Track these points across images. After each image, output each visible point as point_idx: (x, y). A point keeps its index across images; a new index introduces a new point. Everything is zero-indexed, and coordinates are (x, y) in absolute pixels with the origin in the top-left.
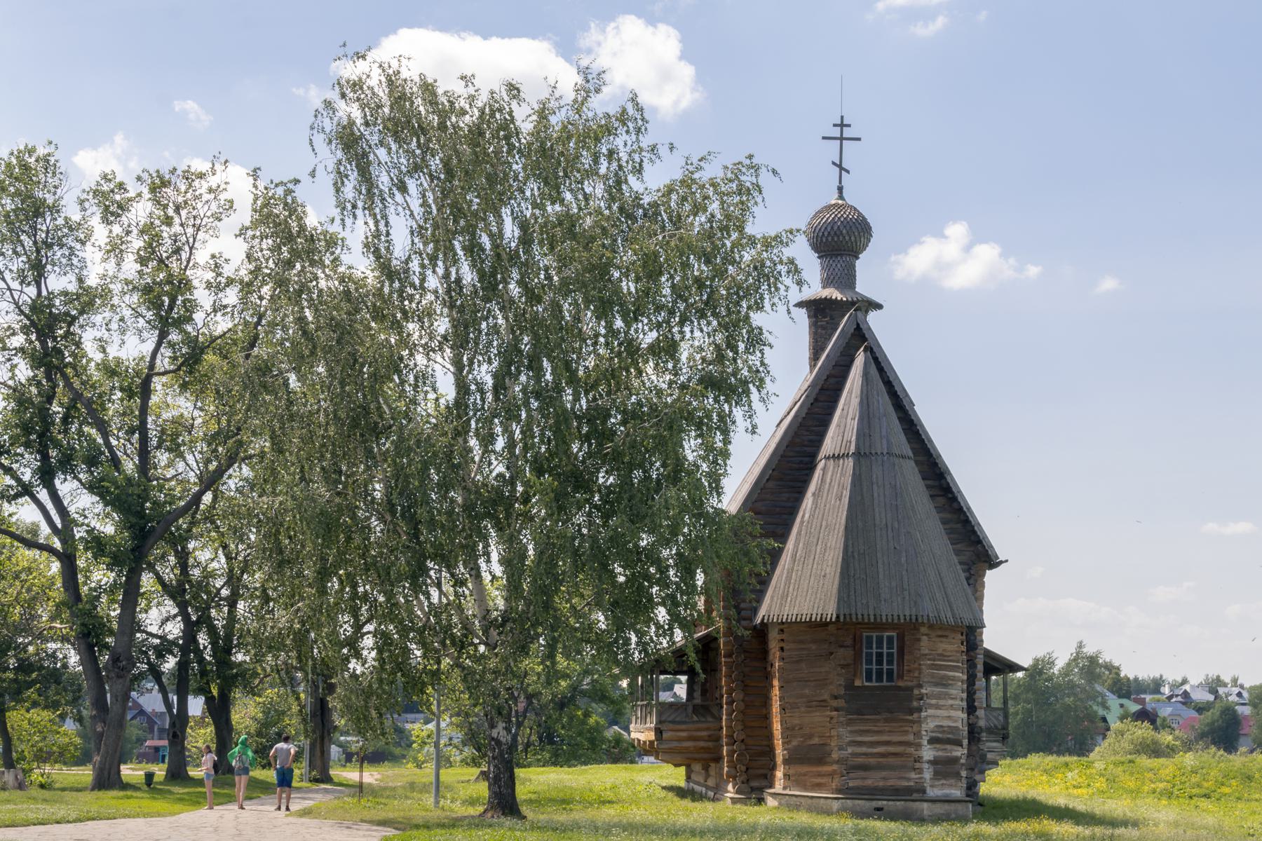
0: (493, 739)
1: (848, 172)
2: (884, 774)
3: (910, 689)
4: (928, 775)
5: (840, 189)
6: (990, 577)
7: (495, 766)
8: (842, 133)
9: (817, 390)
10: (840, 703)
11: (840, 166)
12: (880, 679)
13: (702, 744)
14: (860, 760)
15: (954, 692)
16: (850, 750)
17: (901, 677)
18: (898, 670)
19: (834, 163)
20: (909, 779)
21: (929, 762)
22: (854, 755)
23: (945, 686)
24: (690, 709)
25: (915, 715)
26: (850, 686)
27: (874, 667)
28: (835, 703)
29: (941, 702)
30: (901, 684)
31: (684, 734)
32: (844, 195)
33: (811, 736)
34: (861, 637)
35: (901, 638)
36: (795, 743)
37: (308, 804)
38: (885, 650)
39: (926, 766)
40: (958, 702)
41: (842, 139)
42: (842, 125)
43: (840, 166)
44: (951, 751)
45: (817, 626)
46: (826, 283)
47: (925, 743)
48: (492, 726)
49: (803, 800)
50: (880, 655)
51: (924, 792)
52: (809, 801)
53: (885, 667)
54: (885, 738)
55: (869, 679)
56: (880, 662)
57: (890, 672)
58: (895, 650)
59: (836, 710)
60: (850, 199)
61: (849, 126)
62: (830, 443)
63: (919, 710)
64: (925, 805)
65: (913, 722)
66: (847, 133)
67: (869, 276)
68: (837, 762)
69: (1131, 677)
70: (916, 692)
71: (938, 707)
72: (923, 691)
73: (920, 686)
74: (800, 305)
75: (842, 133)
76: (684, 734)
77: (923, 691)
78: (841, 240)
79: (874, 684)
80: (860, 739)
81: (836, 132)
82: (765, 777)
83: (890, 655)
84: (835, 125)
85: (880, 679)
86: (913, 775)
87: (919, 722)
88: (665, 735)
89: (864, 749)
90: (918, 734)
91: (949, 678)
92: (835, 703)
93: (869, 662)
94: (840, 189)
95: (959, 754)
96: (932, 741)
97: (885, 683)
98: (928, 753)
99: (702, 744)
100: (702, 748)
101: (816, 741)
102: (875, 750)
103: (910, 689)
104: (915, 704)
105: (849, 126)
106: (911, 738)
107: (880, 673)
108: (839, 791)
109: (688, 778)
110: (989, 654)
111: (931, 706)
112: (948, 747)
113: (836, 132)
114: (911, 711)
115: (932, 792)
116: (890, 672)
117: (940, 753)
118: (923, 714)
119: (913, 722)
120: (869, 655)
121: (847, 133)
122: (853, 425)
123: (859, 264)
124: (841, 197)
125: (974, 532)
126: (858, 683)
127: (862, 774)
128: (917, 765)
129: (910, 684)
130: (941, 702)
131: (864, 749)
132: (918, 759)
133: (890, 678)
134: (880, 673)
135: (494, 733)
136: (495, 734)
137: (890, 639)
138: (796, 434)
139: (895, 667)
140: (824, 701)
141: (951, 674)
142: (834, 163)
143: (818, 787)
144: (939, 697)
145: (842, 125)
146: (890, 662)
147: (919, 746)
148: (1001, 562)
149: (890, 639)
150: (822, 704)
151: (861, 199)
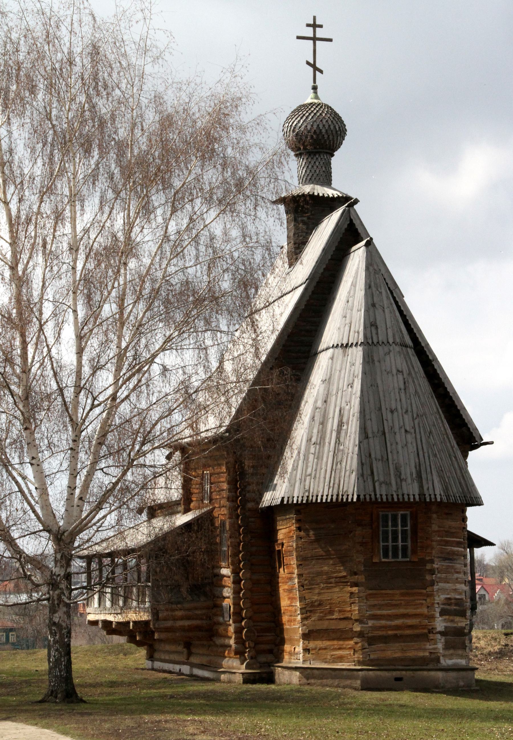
4: (440, 646)
6: (472, 455)
9: (314, 284)
11: (313, 66)
12: (395, 555)
15: (458, 566)
17: (414, 552)
20: (425, 650)
21: (442, 633)
22: (374, 628)
23: (451, 560)
29: (449, 576)
32: (319, 94)
35: (414, 517)
37: (376, 602)
39: (439, 636)
41: (314, 39)
42: (314, 26)
43: (313, 66)
44: (457, 623)
47: (438, 615)
50: (395, 533)
51: (438, 660)
54: (402, 611)
55: (386, 555)
56: (395, 539)
57: (405, 549)
58: (408, 528)
60: (325, 98)
61: (321, 26)
62: (332, 332)
63: (432, 583)
66: (320, 33)
67: (347, 172)
77: (435, 566)
78: (318, 138)
79: (390, 560)
80: (379, 612)
81: (309, 32)
82: (271, 651)
83: (404, 532)
84: (308, 25)
85: (395, 555)
87: (431, 595)
89: (383, 622)
91: (454, 553)
93: (385, 539)
94: (315, 88)
95: (463, 624)
96: (443, 613)
97: (400, 559)
105: (321, 26)
106: (425, 611)
107: (395, 549)
110: (471, 534)
111: (442, 580)
113: (309, 32)
115: (446, 662)
116: (405, 549)
117: (449, 624)
118: (436, 587)
120: (386, 533)
121: (320, 33)
122: (358, 318)
123: (333, 160)
124: (317, 97)
125: (461, 416)
126: (376, 560)
128: (431, 636)
131: (383, 622)
132: (432, 631)
134: (395, 549)
137: (404, 517)
138: (296, 326)
142: (308, 63)
144: (447, 570)
146: (404, 540)
147: (432, 617)
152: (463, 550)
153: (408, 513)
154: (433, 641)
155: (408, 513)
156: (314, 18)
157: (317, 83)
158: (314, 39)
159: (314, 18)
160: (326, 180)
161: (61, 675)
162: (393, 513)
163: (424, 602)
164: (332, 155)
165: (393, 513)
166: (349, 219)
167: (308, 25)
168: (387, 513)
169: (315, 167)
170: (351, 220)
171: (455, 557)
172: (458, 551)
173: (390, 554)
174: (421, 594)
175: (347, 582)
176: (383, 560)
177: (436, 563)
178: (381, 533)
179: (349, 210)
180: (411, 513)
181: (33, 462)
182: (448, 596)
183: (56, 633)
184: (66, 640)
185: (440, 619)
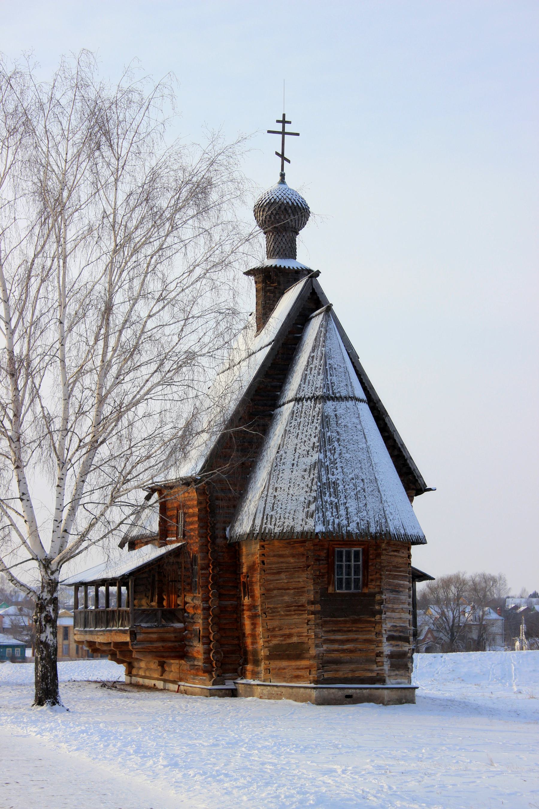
0: (41, 642)
1: (289, 161)
2: (353, 666)
3: (373, 595)
4: (386, 667)
5: (283, 176)
7: (43, 666)
8: (283, 129)
10: (318, 607)
11: (282, 156)
12: (348, 587)
13: (170, 644)
14: (334, 655)
15: (403, 597)
16: (325, 647)
17: (365, 585)
18: (363, 580)
19: (277, 154)
20: (372, 671)
22: (329, 651)
24: (159, 613)
25: (378, 617)
26: (324, 593)
27: (344, 577)
28: (312, 608)
29: (396, 606)
30: (366, 591)
31: (154, 636)
32: (286, 180)
33: (290, 636)
34: (334, 551)
35: (366, 552)
36: (275, 642)
38: (353, 563)
39: (385, 659)
40: (406, 606)
41: (283, 133)
42: (284, 122)
43: (282, 156)
45: (414, 543)
46: (271, 254)
48: (41, 631)
49: (283, 690)
50: (349, 567)
52: (290, 690)
53: (353, 577)
58: (360, 563)
59: (313, 613)
60: (293, 183)
61: (289, 122)
62: (293, 387)
63: (380, 612)
64: (386, 692)
65: (376, 623)
66: (288, 128)
67: (310, 249)
68: (314, 657)
69: (509, 586)
70: (378, 597)
71: (393, 611)
72: (384, 597)
73: (381, 593)
74: (248, 273)
75: (283, 129)
76: (154, 636)
77: (384, 597)
79: (344, 591)
80: (333, 637)
81: (279, 127)
83: (357, 567)
84: (278, 121)
86: (375, 667)
88: (139, 637)
90: (379, 634)
91: (400, 585)
92: (312, 608)
94: (283, 176)
95: (406, 649)
96: (391, 638)
98: (387, 648)
99: (170, 644)
100: (169, 648)
101: (295, 639)
102: (345, 647)
103: (373, 595)
104: (377, 607)
105: (289, 122)
106: (373, 636)
107: (348, 582)
108: (316, 682)
109: (129, 673)
112: (400, 643)
113: (279, 127)
114: (374, 613)
117: (395, 649)
119: (376, 623)
121: (288, 128)
123: (298, 238)
126: (330, 590)
127: (334, 667)
128: (379, 659)
129: (372, 590)
130: (396, 606)
131: (336, 646)
132: (379, 654)
133: (356, 587)
134: (348, 582)
135: (43, 637)
136: (43, 639)
137: (357, 553)
139: (361, 577)
140: (303, 606)
141: (402, 582)
142: (277, 154)
143: (297, 678)
145: (284, 122)
146: (356, 573)
148: (430, 490)
149: (357, 553)
150: (300, 608)
151: (302, 184)
152: (408, 583)
153: (360, 549)
154: (380, 664)
155: (360, 549)
156: (284, 115)
157: (285, 171)
158: (283, 133)
159: (284, 115)
160: (292, 254)
161: (47, 688)
162: (347, 549)
163: (373, 629)
164: (297, 234)
165: (347, 549)
166: (311, 287)
167: (278, 121)
168: (342, 549)
169: (282, 243)
170: (313, 289)
171: (401, 589)
172: (403, 584)
173: (344, 585)
174: (370, 622)
175: (305, 610)
176: (338, 591)
177: (384, 594)
178: (336, 567)
179: (312, 280)
180: (363, 549)
181: (24, 497)
182: (394, 624)
183: (42, 651)
184: (53, 657)
185: (387, 643)
